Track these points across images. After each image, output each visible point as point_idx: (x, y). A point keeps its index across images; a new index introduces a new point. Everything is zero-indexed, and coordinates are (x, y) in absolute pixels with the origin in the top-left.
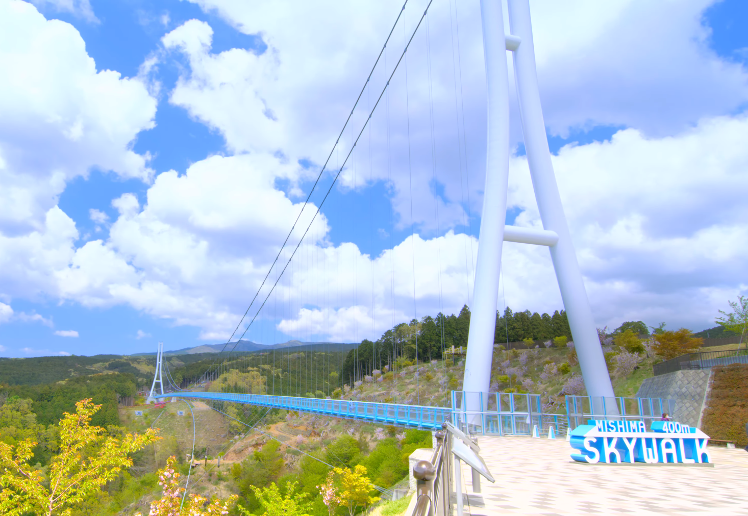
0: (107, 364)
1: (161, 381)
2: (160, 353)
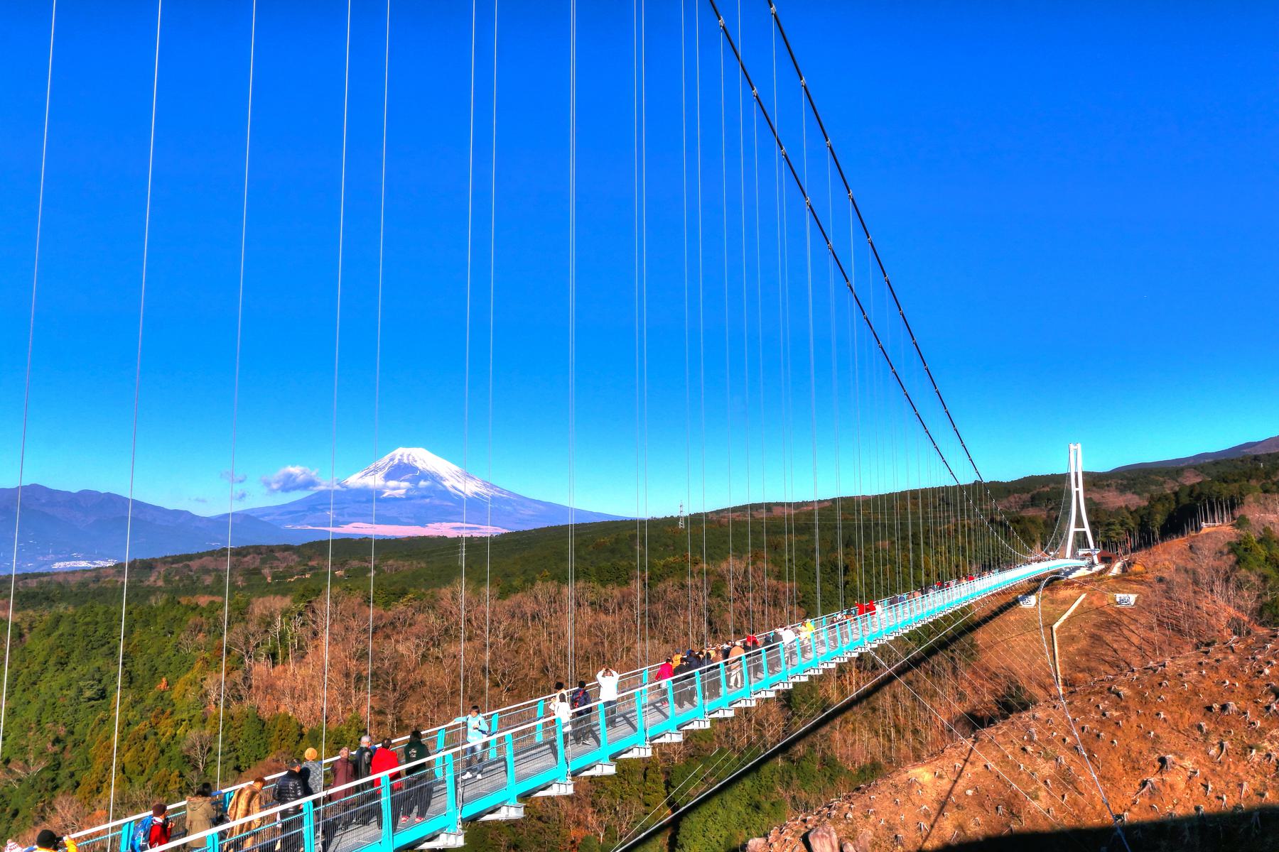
0: (1026, 496)
1: (1087, 529)
2: (1076, 474)
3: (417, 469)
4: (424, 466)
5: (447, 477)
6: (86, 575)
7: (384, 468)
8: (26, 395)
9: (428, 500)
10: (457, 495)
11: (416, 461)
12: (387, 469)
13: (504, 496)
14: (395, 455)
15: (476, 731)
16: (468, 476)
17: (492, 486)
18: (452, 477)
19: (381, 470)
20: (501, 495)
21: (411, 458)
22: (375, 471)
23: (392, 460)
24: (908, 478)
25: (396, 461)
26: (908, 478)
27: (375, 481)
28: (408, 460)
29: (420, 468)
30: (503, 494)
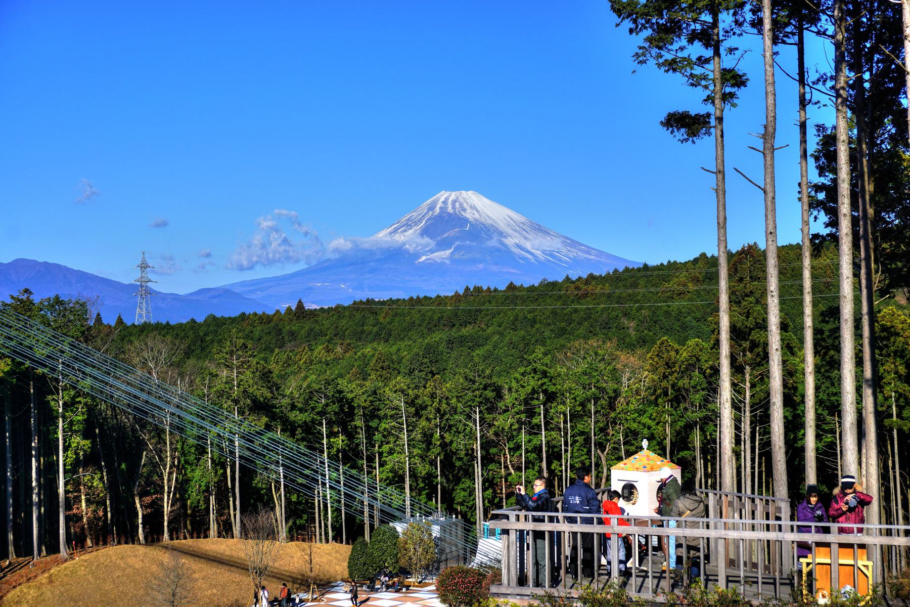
3: (466, 220)
4: (477, 216)
5: (510, 231)
6: (7, 563)
7: (420, 221)
8: (833, 576)
9: (481, 266)
10: (524, 258)
11: (464, 210)
12: (424, 222)
13: (592, 257)
14: (435, 203)
15: (141, 255)
16: (540, 229)
17: (573, 244)
18: (516, 231)
19: (416, 224)
20: (587, 256)
21: (457, 205)
22: (408, 225)
23: (432, 208)
24: (722, 206)
25: (437, 210)
26: (722, 206)
27: (408, 238)
28: (454, 208)
29: (471, 219)
30: (591, 254)
